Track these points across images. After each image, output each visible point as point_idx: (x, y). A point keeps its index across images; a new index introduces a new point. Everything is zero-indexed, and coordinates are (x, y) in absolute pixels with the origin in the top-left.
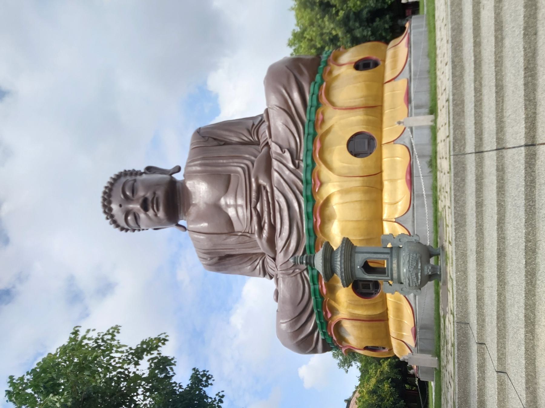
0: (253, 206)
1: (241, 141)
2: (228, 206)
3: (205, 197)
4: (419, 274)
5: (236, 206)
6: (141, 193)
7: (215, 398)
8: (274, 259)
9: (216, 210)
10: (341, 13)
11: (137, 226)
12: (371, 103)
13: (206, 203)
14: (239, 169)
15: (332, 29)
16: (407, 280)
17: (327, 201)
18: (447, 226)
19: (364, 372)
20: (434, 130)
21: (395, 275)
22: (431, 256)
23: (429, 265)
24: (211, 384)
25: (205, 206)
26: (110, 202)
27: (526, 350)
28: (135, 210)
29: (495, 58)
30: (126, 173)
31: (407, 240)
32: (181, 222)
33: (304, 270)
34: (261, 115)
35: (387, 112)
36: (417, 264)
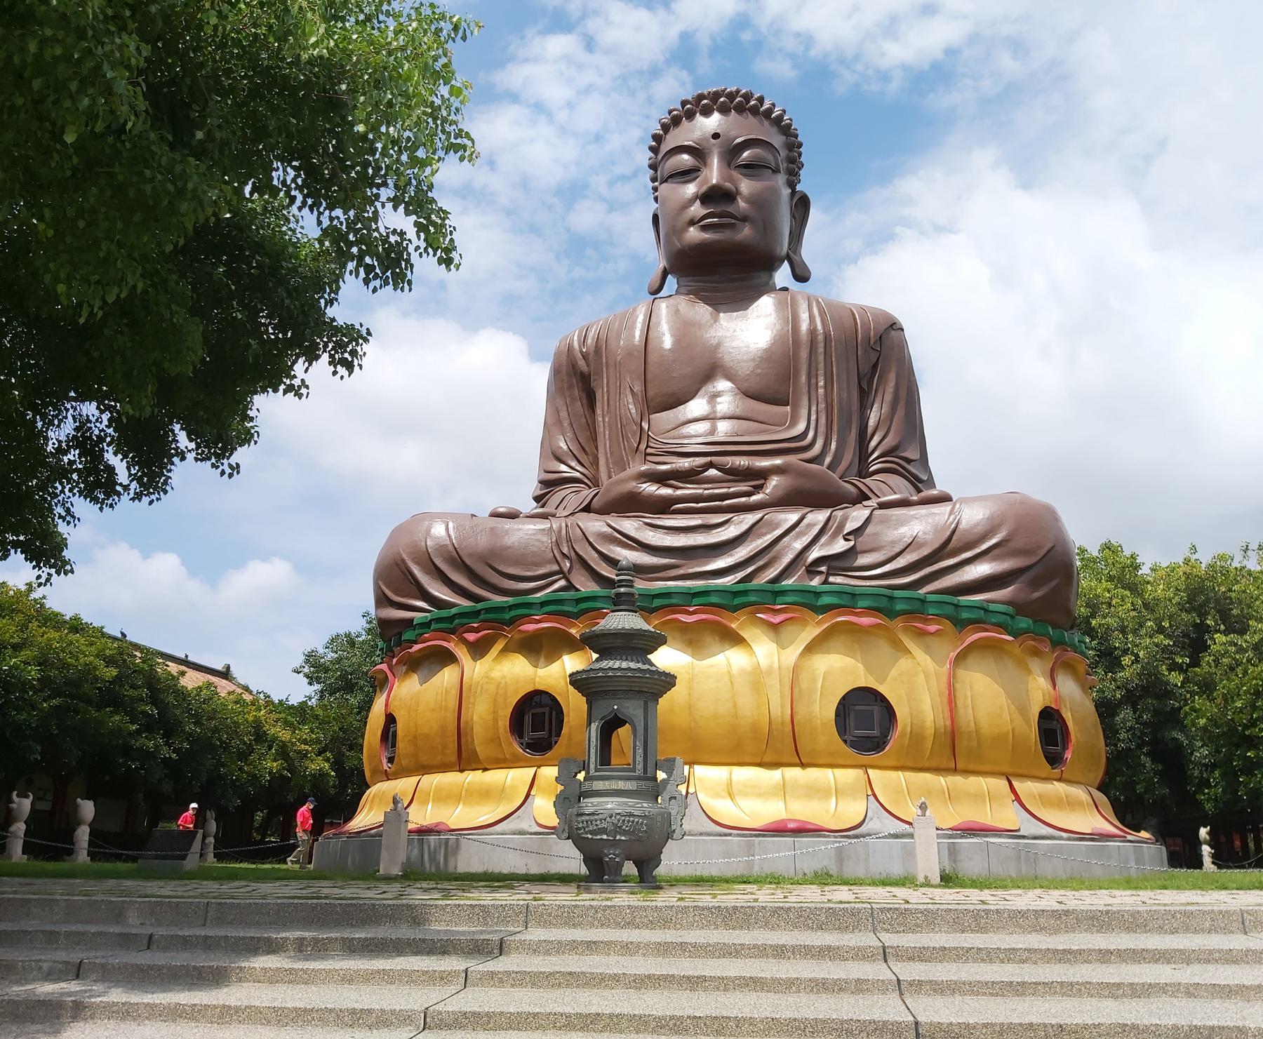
0: (714, 459)
1: (870, 430)
2: (714, 396)
3: (735, 344)
4: (605, 837)
5: (710, 418)
6: (746, 186)
7: (295, 377)
8: (587, 509)
9: (708, 370)
10: (1176, 678)
11: (666, 174)
12: (962, 745)
13: (718, 345)
14: (801, 427)
15: (1137, 656)
16: (592, 810)
17: (736, 639)
18: (714, 896)
19: (301, 711)
20: (906, 881)
21: (599, 785)
22: (638, 864)
23: (620, 857)
24: (335, 373)
25: (714, 342)
26: (724, 110)
27: (536, 1015)
28: (705, 172)
29: (1077, 983)
30: (794, 146)
31: (673, 812)
32: (671, 281)
33: (568, 580)
34: (931, 483)
35: (942, 781)
36: (625, 833)
